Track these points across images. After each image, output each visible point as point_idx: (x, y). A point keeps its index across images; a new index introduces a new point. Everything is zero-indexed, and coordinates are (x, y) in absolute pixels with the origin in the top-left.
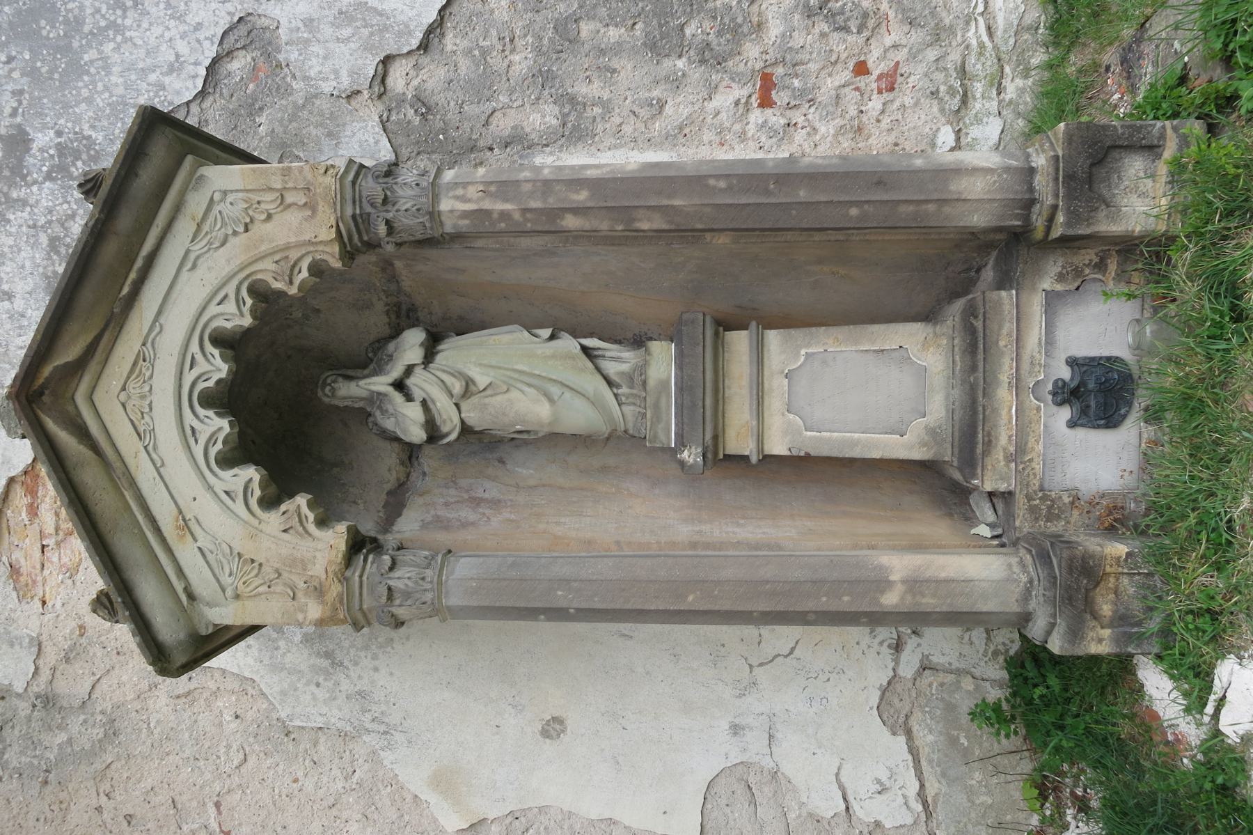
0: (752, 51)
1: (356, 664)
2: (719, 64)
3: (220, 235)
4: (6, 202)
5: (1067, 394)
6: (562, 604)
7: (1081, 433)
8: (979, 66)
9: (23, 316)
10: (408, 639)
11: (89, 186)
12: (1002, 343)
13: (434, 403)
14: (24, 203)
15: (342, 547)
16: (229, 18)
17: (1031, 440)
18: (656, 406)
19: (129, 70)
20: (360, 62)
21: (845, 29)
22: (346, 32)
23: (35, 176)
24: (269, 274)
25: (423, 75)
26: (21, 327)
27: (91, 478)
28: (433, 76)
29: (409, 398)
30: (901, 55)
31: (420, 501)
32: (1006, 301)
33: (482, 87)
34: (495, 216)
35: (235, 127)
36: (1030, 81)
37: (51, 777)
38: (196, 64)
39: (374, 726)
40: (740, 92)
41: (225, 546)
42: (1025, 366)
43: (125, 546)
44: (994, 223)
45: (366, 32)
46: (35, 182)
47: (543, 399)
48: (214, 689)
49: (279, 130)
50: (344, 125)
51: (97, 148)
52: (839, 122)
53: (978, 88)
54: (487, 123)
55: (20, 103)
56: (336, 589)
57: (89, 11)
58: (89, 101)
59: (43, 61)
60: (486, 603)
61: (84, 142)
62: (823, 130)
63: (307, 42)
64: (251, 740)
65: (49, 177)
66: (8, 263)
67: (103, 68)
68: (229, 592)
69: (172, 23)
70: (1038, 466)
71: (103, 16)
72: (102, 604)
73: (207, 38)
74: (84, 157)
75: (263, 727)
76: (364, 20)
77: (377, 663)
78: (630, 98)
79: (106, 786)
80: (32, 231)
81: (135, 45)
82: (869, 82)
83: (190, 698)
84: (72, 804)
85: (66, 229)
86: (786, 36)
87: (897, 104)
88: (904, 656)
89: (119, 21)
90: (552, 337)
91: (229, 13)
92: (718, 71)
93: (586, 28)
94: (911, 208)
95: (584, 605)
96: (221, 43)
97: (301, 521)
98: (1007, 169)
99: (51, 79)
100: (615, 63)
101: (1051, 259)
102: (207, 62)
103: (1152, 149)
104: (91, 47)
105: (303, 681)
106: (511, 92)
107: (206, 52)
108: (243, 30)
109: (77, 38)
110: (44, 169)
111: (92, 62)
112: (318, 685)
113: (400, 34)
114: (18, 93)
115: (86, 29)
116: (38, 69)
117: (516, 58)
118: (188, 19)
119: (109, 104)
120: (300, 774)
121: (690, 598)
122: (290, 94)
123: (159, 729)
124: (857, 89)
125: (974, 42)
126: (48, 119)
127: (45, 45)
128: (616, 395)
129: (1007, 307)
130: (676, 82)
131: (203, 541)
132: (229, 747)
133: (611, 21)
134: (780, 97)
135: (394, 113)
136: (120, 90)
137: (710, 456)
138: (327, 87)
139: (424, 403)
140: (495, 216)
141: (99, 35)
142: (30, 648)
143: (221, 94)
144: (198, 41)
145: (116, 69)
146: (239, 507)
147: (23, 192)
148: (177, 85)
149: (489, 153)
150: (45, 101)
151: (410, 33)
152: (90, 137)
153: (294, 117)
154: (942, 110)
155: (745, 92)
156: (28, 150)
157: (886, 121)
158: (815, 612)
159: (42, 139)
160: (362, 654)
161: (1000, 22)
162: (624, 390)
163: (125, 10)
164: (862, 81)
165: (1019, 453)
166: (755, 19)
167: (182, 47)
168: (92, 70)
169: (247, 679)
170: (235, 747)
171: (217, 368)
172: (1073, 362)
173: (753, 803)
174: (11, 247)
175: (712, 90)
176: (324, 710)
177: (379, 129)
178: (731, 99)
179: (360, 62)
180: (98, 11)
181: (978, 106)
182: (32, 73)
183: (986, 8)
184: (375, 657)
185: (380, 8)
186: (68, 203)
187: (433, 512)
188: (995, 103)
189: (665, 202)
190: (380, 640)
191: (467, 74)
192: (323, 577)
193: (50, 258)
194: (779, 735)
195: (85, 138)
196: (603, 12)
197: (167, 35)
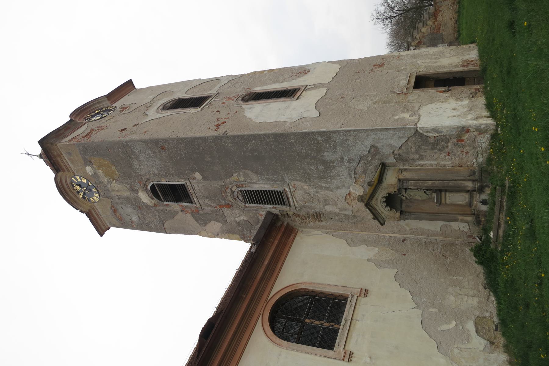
0: (446, 150)
7: (483, 205)
21: (460, 147)
25: (399, 151)
27: (373, 210)
28: (401, 152)
30: (468, 150)
36: (487, 154)
38: (367, 150)
40: (445, 154)
49: (379, 158)
52: (459, 158)
53: (479, 155)
54: (409, 157)
62: (457, 159)
65: (347, 162)
70: (478, 208)
72: (373, 218)
79: (363, 224)
87: (468, 156)
98: (473, 187)
103: (489, 187)
106: (412, 154)
114: (341, 153)
117: (412, 149)
125: (479, 150)
131: (384, 214)
133: (426, 146)
134: (450, 155)
138: (386, 153)
141: (352, 146)
145: (355, 150)
146: (388, 211)
148: (364, 152)
154: (474, 157)
155: (445, 154)
161: (483, 147)
162: (429, 195)
165: (476, 206)
166: (447, 146)
167: (365, 148)
172: (482, 199)
175: (441, 154)
177: (393, 158)
178: (443, 155)
181: (479, 157)
182: (343, 150)
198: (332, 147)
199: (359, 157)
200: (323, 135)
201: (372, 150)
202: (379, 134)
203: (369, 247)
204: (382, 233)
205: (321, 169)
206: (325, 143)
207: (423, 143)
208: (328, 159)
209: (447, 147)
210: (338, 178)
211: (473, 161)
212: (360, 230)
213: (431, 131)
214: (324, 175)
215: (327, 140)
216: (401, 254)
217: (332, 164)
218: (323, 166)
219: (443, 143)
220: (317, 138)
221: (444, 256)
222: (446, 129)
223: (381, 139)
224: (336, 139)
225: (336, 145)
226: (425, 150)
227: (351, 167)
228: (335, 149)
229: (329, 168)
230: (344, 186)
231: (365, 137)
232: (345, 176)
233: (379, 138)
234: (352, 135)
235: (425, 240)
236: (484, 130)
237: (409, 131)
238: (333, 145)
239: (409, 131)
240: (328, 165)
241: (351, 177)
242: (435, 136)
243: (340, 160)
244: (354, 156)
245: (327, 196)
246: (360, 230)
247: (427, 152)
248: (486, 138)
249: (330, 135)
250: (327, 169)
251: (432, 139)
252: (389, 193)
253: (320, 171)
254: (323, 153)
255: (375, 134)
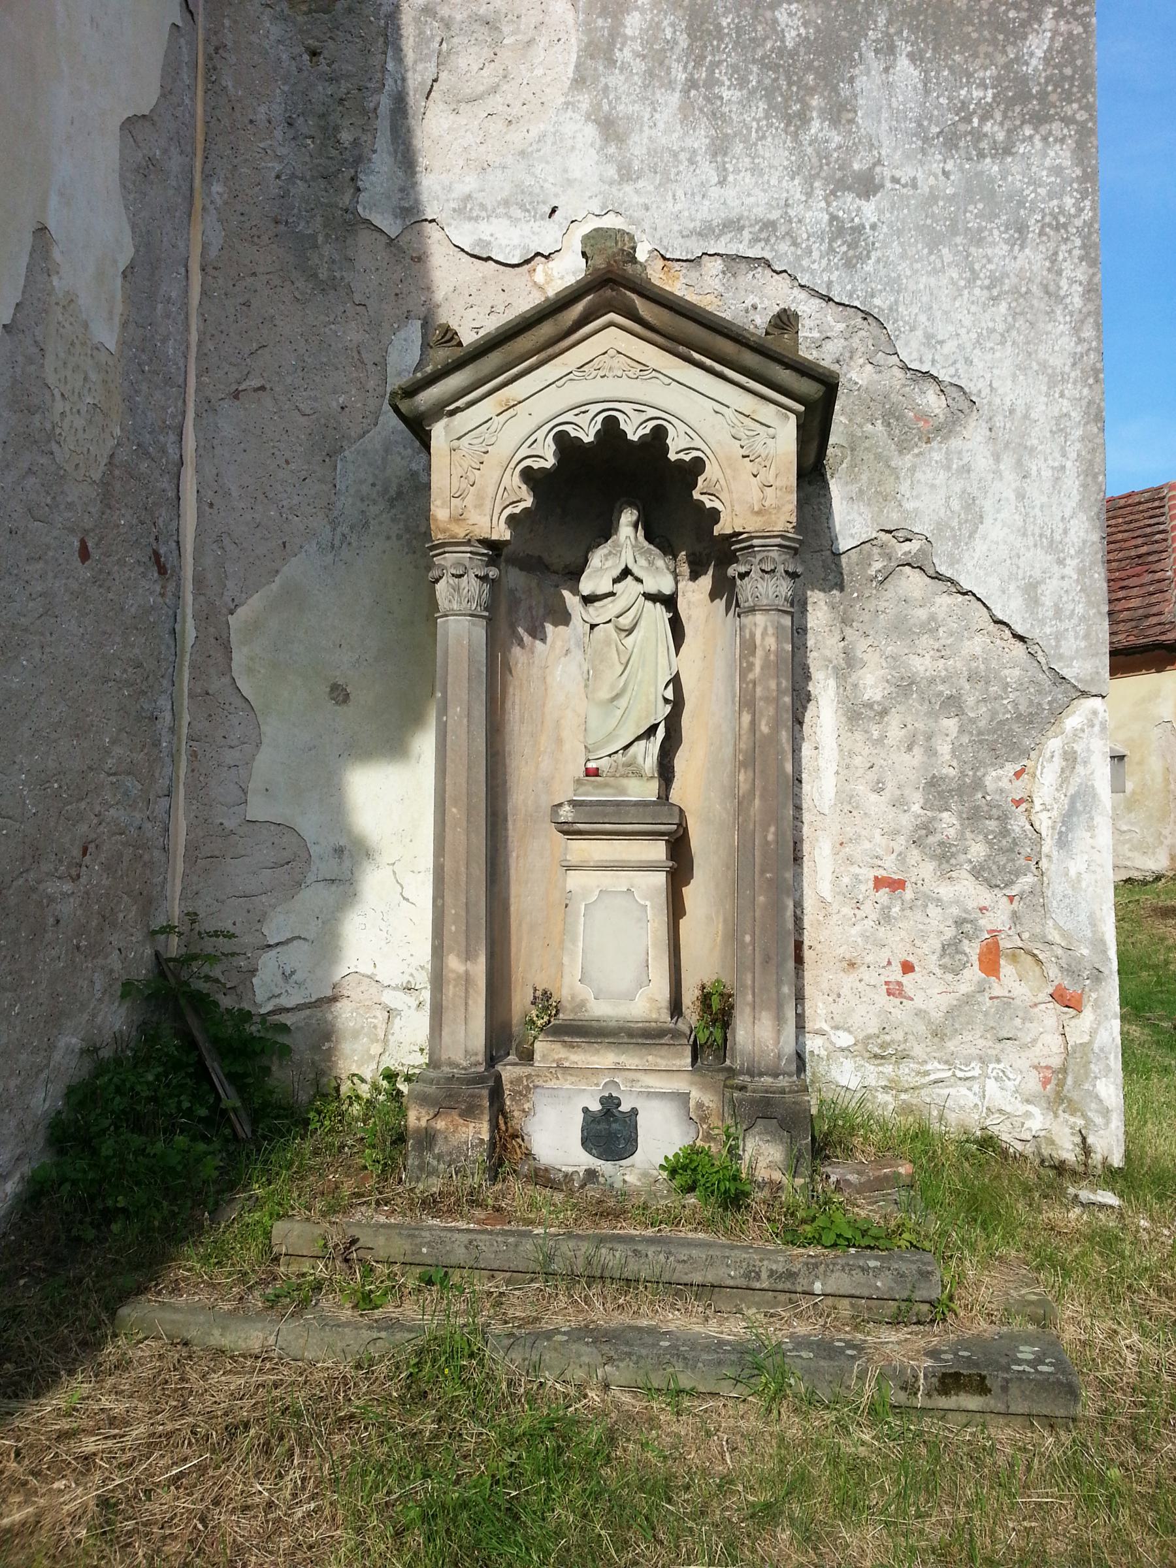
1: (393, 520)
2: (914, 842)
3: (741, 435)
4: (810, 175)
5: (610, 1104)
6: (450, 712)
7: (579, 1118)
8: (907, 1071)
9: (704, 196)
10: (416, 567)
11: (785, 319)
12: (650, 1058)
13: (612, 602)
14: (809, 195)
15: (495, 537)
16: (975, 391)
17: (573, 1079)
18: (606, 785)
19: (931, 294)
20: (927, 519)
22: (956, 505)
23: (835, 204)
24: (711, 471)
26: (693, 194)
29: (616, 581)
31: (534, 584)
32: (683, 1063)
33: (901, 629)
34: (751, 659)
35: (872, 400)
37: (282, 228)
39: (338, 537)
41: (494, 439)
42: (631, 1075)
43: (494, 359)
44: (738, 1047)
45: (955, 524)
46: (828, 204)
47: (614, 693)
48: (367, 387)
50: (869, 505)
51: (859, 266)
53: (888, 1069)
55: (904, 186)
56: (460, 532)
57: (989, 251)
58: (903, 256)
59: (944, 208)
60: (450, 650)
61: (865, 253)
63: (949, 468)
64: (323, 421)
65: (833, 218)
66: (753, 180)
67: (934, 269)
68: (456, 443)
69: (974, 336)
70: (552, 1084)
71: (984, 266)
73: (957, 370)
74: (851, 253)
75: (334, 432)
76: (966, 521)
77: (394, 538)
78: (885, 763)
80: (782, 203)
81: (955, 299)
82: (895, 974)
83: (358, 363)
84: (257, 248)
85: (783, 237)
86: (938, 902)
88: (400, 995)
89: (979, 283)
90: (666, 701)
91: (980, 391)
92: (907, 841)
93: (951, 725)
94: (749, 982)
95: (449, 728)
96: (951, 384)
97: (514, 502)
99: (926, 217)
100: (917, 750)
101: (715, 1098)
102: (934, 372)
104: (955, 255)
105: (377, 472)
107: (944, 371)
108: (965, 405)
109: (965, 241)
110: (841, 213)
111: (941, 257)
112: (373, 485)
113: (951, 555)
115: (973, 250)
116: (936, 203)
118: (977, 351)
119: (899, 276)
120: (293, 466)
121: (454, 810)
122: (900, 452)
123: (329, 333)
124: (889, 963)
125: (929, 1067)
126: (888, 215)
127: (959, 209)
128: (616, 752)
129: (678, 1062)
130: (899, 803)
132: (315, 399)
134: (883, 895)
135: (879, 550)
136: (912, 286)
137: (565, 827)
139: (612, 594)
140: (751, 659)
142: (400, 208)
143: (904, 386)
144: (955, 362)
147: (819, 193)
148: (914, 344)
149: (839, 637)
150: (906, 211)
151: (951, 565)
152: (869, 258)
153: (878, 457)
156: (859, 196)
157: (861, 986)
158: (443, 905)
159: (869, 210)
160: (401, 525)
163: (988, 288)
164: (897, 968)
165: (563, 1069)
167: (950, 347)
168: (933, 258)
169: (377, 418)
170: (315, 405)
171: (635, 430)
172: (634, 1112)
173: (276, 866)
174: (768, 182)
176: (352, 491)
177: (864, 538)
179: (927, 519)
180: (990, 261)
182: (933, 198)
183: (960, 1079)
184: (399, 537)
185: (977, 536)
186: (808, 239)
187: (523, 597)
188: (873, 1084)
189: (757, 793)
190: (414, 542)
191: (912, 617)
192: (471, 522)
193: (757, 222)
194: (334, 888)
195: (869, 252)
196: (965, 739)
197: (963, 331)
198: (962, 127)
199: (877, 301)
200: (1068, 71)
201: (932, 401)
202: (1064, 455)
203: (119, 281)
204: (198, 415)
205: (775, 21)
206: (998, 81)
207: (980, 733)
208: (862, 82)
209: (946, 876)
210: (700, 139)
211: (837, 1028)
212: (213, 253)
213: (1075, 781)
214: (721, 40)
215: (1023, 97)
216: (88, 523)
217: (822, 111)
218: (804, 41)
219: (978, 850)
220: (1041, 23)
221: (85, 851)
222: (1084, 876)
223: (1019, 463)
224: (1026, 157)
225: (981, 155)
226: (921, 739)
227: (795, 244)
228: (951, 141)
229: (783, 83)
230: (626, 174)
231: (1042, 355)
232: (714, 192)
233: (1032, 450)
234: (1059, 273)
235: (168, 716)
236: (1075, 1095)
237: (1083, 644)
238: (978, 136)
239: (1083, 644)
240: (810, 78)
241: (706, 231)
242: (1037, 807)
243: (856, 166)
244: (883, 272)
245: (530, 43)
246: (213, 253)
247: (910, 749)
248: (1017, 1107)
249: (1067, 121)
250: (775, 68)
251: (1017, 789)
252: (698, 466)
253: (755, 18)
254: (911, 56)
255: (1064, 423)
